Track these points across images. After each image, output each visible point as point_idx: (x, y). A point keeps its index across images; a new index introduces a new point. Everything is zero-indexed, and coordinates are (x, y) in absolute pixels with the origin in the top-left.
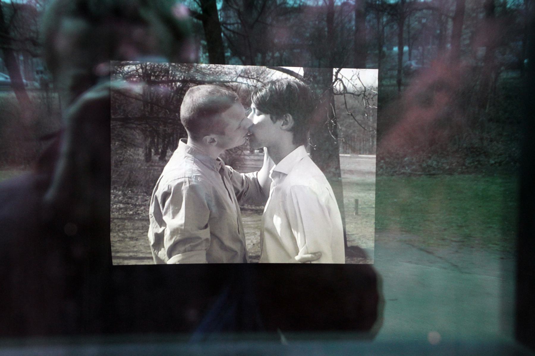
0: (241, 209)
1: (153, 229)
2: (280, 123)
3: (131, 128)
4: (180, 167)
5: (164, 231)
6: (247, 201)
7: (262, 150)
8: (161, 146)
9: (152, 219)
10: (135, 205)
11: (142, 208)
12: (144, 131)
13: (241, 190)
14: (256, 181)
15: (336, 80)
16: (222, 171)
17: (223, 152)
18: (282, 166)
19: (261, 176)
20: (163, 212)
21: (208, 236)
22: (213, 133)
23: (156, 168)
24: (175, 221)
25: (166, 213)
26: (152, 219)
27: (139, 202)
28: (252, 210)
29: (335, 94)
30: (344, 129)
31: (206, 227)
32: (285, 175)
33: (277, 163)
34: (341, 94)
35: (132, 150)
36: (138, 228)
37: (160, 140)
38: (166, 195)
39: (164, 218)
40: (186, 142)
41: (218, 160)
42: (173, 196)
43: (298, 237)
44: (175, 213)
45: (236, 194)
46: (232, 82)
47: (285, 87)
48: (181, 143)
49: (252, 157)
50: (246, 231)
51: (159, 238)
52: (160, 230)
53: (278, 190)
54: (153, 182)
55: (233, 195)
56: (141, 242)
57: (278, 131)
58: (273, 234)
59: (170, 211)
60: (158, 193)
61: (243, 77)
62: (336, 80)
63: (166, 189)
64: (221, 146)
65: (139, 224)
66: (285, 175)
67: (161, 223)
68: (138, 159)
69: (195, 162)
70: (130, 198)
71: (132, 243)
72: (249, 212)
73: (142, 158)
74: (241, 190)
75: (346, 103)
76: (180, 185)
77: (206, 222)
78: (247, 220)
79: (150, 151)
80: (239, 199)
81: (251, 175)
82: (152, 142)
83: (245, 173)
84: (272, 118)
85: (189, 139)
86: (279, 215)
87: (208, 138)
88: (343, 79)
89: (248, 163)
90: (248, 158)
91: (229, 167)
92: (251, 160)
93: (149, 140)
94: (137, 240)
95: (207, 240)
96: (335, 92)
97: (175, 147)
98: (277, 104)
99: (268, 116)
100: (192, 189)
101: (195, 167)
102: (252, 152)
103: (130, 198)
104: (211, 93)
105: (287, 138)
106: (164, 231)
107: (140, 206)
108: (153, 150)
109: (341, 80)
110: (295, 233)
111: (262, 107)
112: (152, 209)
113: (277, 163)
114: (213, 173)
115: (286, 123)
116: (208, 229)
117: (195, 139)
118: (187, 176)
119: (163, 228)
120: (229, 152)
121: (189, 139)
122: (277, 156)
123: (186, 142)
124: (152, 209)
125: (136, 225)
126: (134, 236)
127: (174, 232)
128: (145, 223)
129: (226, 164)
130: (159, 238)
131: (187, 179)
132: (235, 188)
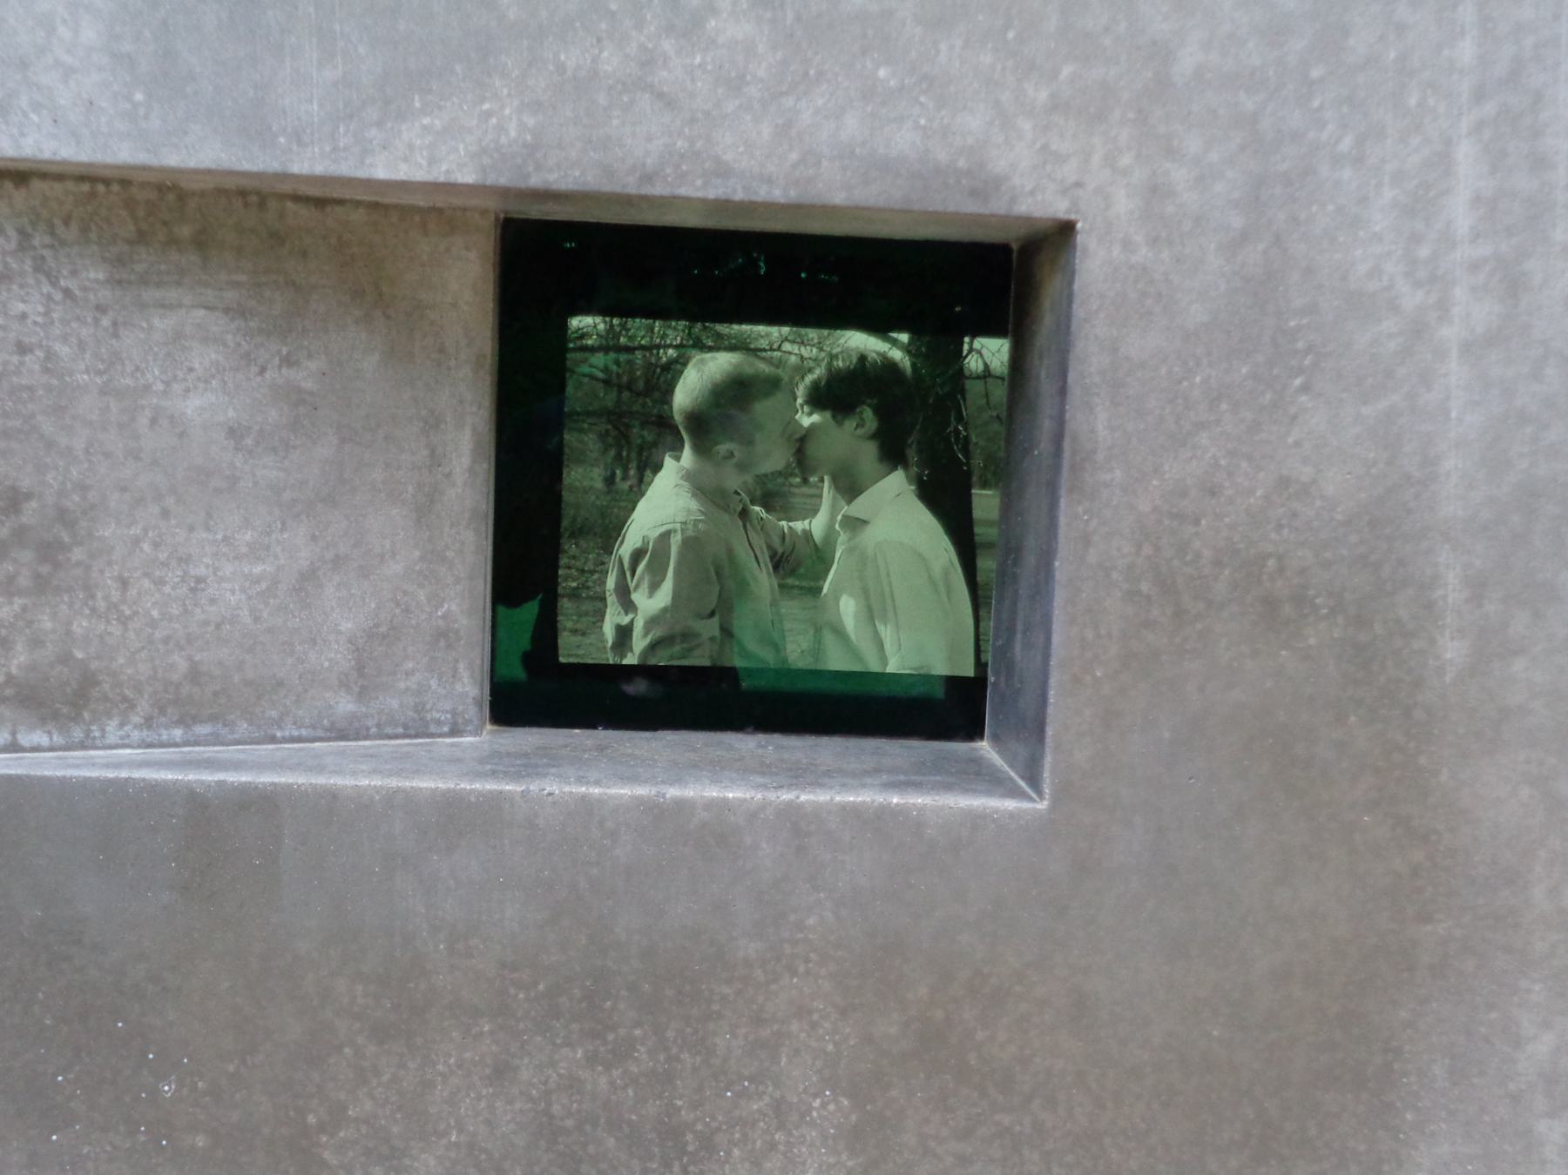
0: (781, 586)
1: (613, 618)
2: (850, 424)
3: (581, 431)
4: (665, 502)
5: (632, 621)
6: (793, 572)
7: (822, 480)
8: (633, 465)
9: (611, 599)
10: (583, 571)
11: (596, 576)
12: (603, 436)
13: (780, 551)
14: (808, 535)
15: (971, 350)
16: (744, 514)
17: (749, 478)
18: (859, 507)
19: (817, 525)
20: (632, 586)
21: (717, 633)
22: (732, 440)
23: (623, 504)
24: (652, 602)
25: (637, 587)
26: (611, 599)
27: (589, 566)
28: (801, 588)
29: (970, 377)
30: (982, 443)
31: (712, 614)
32: (865, 522)
33: (849, 502)
34: (978, 377)
35: (580, 470)
36: (587, 614)
37: (633, 455)
38: (637, 555)
39: (635, 597)
40: (678, 459)
41: (737, 493)
42: (653, 556)
43: (886, 632)
44: (654, 587)
45: (772, 558)
46: (772, 349)
47: (855, 360)
48: (669, 462)
49: (805, 490)
50: (787, 626)
51: (624, 633)
52: (626, 620)
53: (850, 550)
54: (612, 531)
55: (765, 558)
56: (591, 639)
57: (851, 438)
58: (840, 632)
59: (645, 585)
60: (626, 549)
61: (793, 342)
62: (971, 350)
63: (639, 545)
64: (742, 467)
65: (587, 606)
66: (865, 522)
67: (628, 606)
68: (591, 488)
69: (694, 495)
70: (574, 557)
71: (577, 639)
72: (796, 591)
73: (599, 485)
74: (780, 551)
75: (987, 395)
76: (666, 536)
77: (713, 606)
78: (792, 609)
79: (613, 474)
80: (776, 567)
81: (799, 526)
82: (619, 457)
83: (789, 520)
84: (834, 417)
85: (687, 453)
86: (851, 595)
87: (723, 448)
88: (984, 351)
89: (796, 500)
90: (797, 491)
91: (757, 508)
92: (804, 495)
93: (612, 453)
94: (584, 634)
95: (712, 639)
96: (967, 373)
97: (657, 468)
98: (841, 392)
99: (828, 414)
100: (690, 544)
101: (694, 505)
102: (805, 481)
103: (574, 557)
104: (736, 366)
105: (869, 452)
106: (632, 621)
107: (592, 572)
108: (618, 472)
109: (979, 352)
110: (881, 628)
111: (820, 398)
112: (611, 583)
113: (849, 502)
114: (726, 517)
115: (860, 425)
116: (716, 620)
117: (701, 449)
118: (678, 519)
119: (631, 616)
120: (762, 479)
121: (687, 453)
122: (850, 488)
123: (678, 459)
124: (611, 583)
125: (584, 608)
126: (579, 626)
127: (652, 622)
128: (599, 605)
129: (753, 502)
130: (624, 633)
131: (678, 526)
132: (769, 547)
